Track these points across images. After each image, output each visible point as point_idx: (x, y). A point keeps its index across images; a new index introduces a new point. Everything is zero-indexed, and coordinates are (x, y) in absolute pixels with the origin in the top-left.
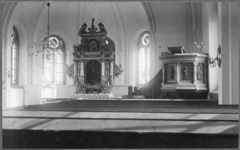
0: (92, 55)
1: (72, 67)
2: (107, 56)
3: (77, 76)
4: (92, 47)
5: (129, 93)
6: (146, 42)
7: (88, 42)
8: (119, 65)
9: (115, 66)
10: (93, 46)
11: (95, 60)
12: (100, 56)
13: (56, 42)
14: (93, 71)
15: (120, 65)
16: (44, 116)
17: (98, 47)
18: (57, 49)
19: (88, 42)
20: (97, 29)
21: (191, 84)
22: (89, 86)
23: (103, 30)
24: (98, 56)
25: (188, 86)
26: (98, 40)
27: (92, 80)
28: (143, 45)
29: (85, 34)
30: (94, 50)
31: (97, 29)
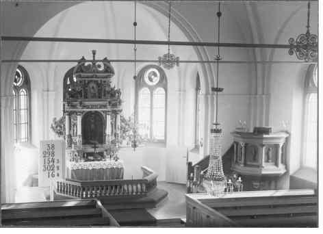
0: (93, 105)
1: (62, 121)
2: (115, 105)
3: (70, 136)
4: (90, 92)
5: (268, 64)
6: (151, 80)
7: (85, 84)
8: (128, 119)
9: (123, 120)
10: (92, 90)
11: (96, 112)
12: (105, 106)
13: (19, 76)
14: (93, 126)
15: (130, 118)
16: (203, 114)
17: (100, 91)
18: (21, 87)
19: (85, 84)
20: (99, 66)
21: (275, 167)
22: (90, 149)
23: (109, 71)
24: (101, 107)
25: (273, 170)
26: (99, 82)
27: (91, 139)
28: (145, 83)
29: (82, 74)
30: (94, 96)
31: (99, 66)
